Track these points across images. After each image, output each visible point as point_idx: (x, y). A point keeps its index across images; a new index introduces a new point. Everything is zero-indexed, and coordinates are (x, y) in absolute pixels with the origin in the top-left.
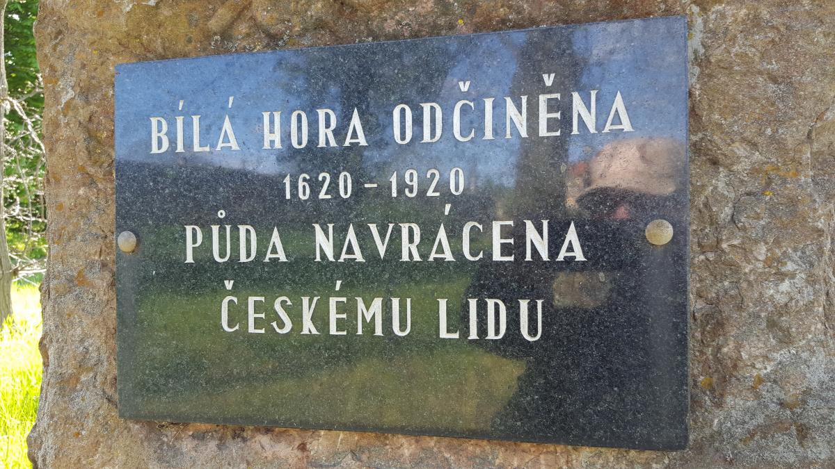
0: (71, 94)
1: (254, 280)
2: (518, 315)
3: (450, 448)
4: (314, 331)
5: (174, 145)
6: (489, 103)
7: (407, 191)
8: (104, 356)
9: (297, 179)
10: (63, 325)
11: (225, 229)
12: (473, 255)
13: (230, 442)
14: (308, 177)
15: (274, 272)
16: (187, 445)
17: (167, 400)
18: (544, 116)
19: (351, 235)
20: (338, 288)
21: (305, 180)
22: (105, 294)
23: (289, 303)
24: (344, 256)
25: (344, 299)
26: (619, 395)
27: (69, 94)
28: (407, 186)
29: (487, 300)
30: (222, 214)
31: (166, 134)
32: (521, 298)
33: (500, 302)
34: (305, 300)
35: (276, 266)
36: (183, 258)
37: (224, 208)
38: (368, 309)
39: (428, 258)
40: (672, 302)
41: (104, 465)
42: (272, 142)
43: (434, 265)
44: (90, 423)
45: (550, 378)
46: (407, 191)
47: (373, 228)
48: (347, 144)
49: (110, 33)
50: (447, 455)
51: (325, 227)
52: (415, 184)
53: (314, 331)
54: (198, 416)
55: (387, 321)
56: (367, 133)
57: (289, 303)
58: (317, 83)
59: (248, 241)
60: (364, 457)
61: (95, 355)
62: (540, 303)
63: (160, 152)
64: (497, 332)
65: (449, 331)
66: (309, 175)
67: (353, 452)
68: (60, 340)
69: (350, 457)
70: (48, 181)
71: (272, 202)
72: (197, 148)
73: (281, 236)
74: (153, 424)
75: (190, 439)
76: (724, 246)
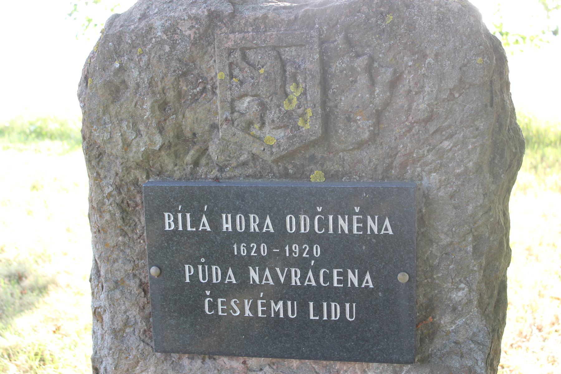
0: (111, 188)
1: (220, 291)
2: (345, 309)
4: (251, 315)
5: (177, 227)
6: (331, 218)
7: (293, 254)
8: (139, 320)
9: (240, 246)
10: (113, 304)
11: (205, 267)
13: (207, 360)
14: (245, 245)
15: (230, 288)
16: (186, 361)
17: (179, 344)
18: (355, 225)
19: (267, 272)
20: (261, 296)
21: (244, 246)
22: (137, 290)
23: (238, 302)
24: (264, 282)
25: (265, 301)
26: (387, 342)
27: (110, 189)
28: (294, 251)
29: (331, 303)
30: (203, 260)
31: (173, 221)
32: (347, 303)
34: (246, 301)
35: (231, 285)
36: (184, 279)
38: (276, 305)
39: (304, 284)
40: (409, 305)
41: (142, 371)
42: (227, 228)
43: (307, 287)
45: (359, 335)
46: (293, 254)
47: (278, 270)
48: (264, 231)
49: (132, 160)
50: (314, 366)
51: (254, 268)
52: (297, 250)
53: (251, 315)
54: (196, 351)
55: (285, 311)
56: (274, 226)
57: (238, 302)
59: (217, 273)
61: (133, 319)
62: (354, 304)
63: (170, 229)
64: (336, 317)
66: (246, 244)
67: (269, 365)
68: (113, 312)
69: (268, 367)
70: (99, 231)
71: (228, 255)
72: (189, 229)
73: (233, 272)
74: (166, 352)
75: (187, 359)
76: (435, 276)
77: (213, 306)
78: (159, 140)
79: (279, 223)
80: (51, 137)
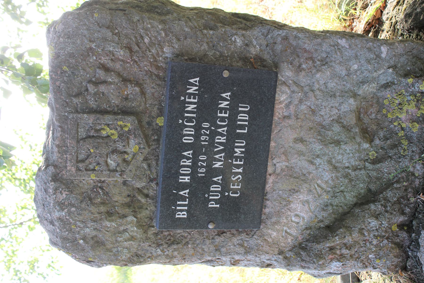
1: (226, 186)
3: (273, 132)
4: (242, 168)
6: (186, 115)
7: (207, 139)
11: (211, 195)
12: (226, 122)
13: (266, 197)
15: (225, 180)
16: (267, 211)
18: (192, 100)
19: (217, 156)
20: (231, 161)
24: (222, 159)
25: (234, 159)
28: (205, 139)
30: (207, 196)
31: (181, 212)
33: (239, 116)
34: (233, 171)
37: (205, 195)
42: (188, 179)
44: (259, 241)
46: (207, 139)
47: (216, 150)
49: (141, 236)
50: (275, 133)
52: (205, 137)
53: (242, 168)
58: (173, 165)
59: (215, 188)
60: (274, 156)
61: (239, 241)
62: (240, 105)
64: (246, 117)
65: (245, 130)
67: (273, 160)
70: (184, 259)
72: (187, 203)
74: (260, 222)
79: (188, 147)
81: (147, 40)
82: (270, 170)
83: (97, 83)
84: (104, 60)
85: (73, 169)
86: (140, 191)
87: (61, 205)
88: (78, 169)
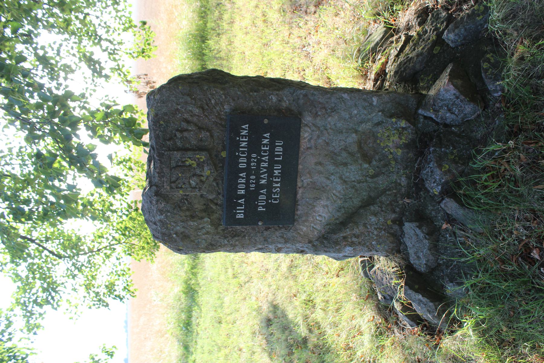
0: (226, 241)
19: (262, 176)
30: (256, 203)
77: (275, 199)
78: (206, 219)
79: (242, 171)
80: (190, 317)
81: (213, 102)
82: (299, 184)
83: (182, 131)
84: (186, 116)
85: (168, 188)
86: (212, 201)
87: (161, 212)
88: (171, 188)
